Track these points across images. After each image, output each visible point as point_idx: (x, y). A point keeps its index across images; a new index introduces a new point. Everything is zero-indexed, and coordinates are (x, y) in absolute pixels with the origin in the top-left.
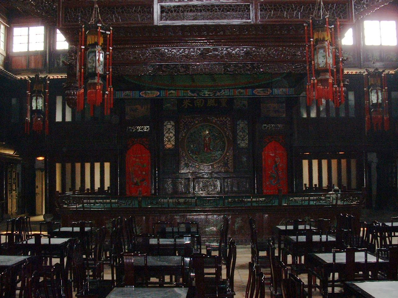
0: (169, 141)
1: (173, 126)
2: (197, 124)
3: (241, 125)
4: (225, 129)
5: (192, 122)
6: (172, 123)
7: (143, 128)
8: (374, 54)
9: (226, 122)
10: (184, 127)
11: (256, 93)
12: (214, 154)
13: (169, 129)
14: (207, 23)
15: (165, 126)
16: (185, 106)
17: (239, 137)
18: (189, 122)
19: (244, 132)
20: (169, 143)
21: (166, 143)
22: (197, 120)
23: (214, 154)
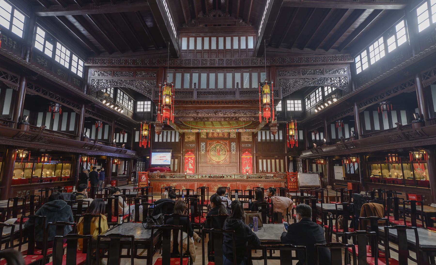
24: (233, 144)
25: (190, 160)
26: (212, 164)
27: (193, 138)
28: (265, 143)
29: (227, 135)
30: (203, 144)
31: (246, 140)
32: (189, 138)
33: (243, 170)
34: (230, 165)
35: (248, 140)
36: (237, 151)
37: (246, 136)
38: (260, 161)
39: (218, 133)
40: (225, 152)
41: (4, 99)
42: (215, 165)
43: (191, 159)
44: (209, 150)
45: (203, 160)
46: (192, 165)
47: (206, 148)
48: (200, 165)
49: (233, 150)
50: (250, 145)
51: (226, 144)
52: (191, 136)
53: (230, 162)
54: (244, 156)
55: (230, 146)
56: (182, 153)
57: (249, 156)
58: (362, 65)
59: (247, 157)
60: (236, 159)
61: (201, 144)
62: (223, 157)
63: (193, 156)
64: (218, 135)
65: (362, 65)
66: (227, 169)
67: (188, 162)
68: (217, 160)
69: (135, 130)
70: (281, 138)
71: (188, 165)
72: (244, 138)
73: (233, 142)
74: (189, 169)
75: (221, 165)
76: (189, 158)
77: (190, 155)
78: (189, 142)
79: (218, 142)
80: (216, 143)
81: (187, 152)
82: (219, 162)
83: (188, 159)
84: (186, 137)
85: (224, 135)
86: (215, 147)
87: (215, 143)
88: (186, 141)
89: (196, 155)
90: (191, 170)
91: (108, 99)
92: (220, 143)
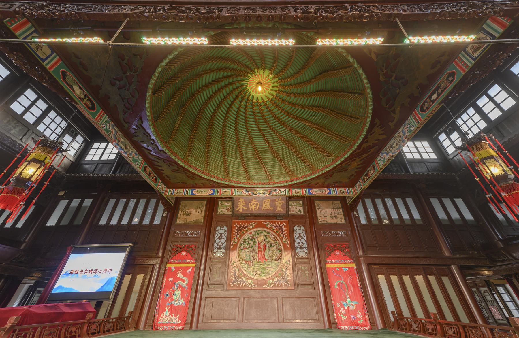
0: (301, 248)
1: (303, 231)
2: (251, 229)
3: (299, 231)
4: (282, 235)
5: (246, 227)
6: (225, 228)
7: (193, 233)
8: (477, 153)
9: (281, 227)
10: (237, 233)
11: (314, 193)
12: (269, 265)
13: (221, 234)
14: (65, 87)
15: (218, 231)
16: (240, 209)
17: (297, 245)
18: (243, 227)
19: (302, 238)
20: (302, 250)
21: (216, 250)
22: (252, 225)
23: (269, 265)
24: (299, 230)
25: (180, 275)
26: (242, 289)
27: (196, 214)
28: (375, 229)
29: (282, 207)
30: (221, 231)
31: (330, 220)
32: (188, 215)
33: (338, 310)
34: (297, 293)
35: (334, 221)
36: (310, 249)
37: (329, 211)
38: (382, 279)
39: (261, 201)
40: (280, 250)
41: (434, 210)
42: (252, 294)
43: (184, 274)
44: (236, 246)
45: (216, 278)
46: (182, 296)
47: (229, 239)
48: (206, 293)
49: (301, 248)
50: (342, 233)
51: (280, 228)
52: (193, 211)
53: (296, 284)
54: (331, 265)
55: (291, 235)
56: (160, 254)
57: (348, 265)
58: (105, 149)
59: (339, 265)
60: (312, 274)
61: (215, 231)
62: (273, 268)
63: (191, 265)
64: (261, 205)
65: (105, 149)
66: (288, 305)
67: (173, 283)
68: (257, 277)
69: (62, 198)
70: (416, 216)
71: (172, 294)
72: (327, 214)
73: (299, 225)
74: (173, 310)
75: (270, 294)
76: (178, 269)
77: (183, 260)
78: (187, 226)
79: (260, 225)
80: (256, 227)
81: (177, 251)
82: (265, 282)
83: (174, 275)
84: (181, 212)
85: (275, 207)
86: (253, 239)
87: (252, 230)
88: (179, 221)
89: (198, 261)
90: (177, 313)
91: (88, 330)
92: (264, 226)
